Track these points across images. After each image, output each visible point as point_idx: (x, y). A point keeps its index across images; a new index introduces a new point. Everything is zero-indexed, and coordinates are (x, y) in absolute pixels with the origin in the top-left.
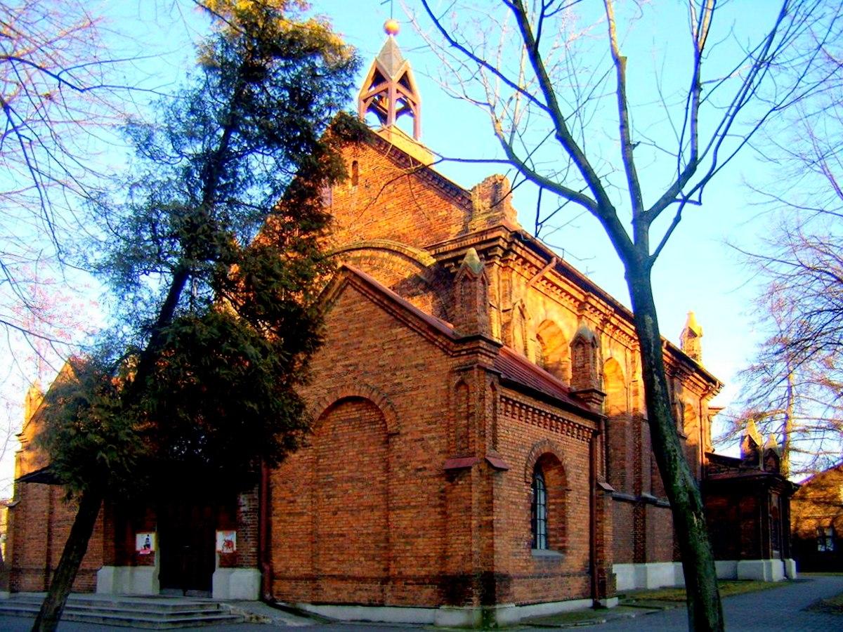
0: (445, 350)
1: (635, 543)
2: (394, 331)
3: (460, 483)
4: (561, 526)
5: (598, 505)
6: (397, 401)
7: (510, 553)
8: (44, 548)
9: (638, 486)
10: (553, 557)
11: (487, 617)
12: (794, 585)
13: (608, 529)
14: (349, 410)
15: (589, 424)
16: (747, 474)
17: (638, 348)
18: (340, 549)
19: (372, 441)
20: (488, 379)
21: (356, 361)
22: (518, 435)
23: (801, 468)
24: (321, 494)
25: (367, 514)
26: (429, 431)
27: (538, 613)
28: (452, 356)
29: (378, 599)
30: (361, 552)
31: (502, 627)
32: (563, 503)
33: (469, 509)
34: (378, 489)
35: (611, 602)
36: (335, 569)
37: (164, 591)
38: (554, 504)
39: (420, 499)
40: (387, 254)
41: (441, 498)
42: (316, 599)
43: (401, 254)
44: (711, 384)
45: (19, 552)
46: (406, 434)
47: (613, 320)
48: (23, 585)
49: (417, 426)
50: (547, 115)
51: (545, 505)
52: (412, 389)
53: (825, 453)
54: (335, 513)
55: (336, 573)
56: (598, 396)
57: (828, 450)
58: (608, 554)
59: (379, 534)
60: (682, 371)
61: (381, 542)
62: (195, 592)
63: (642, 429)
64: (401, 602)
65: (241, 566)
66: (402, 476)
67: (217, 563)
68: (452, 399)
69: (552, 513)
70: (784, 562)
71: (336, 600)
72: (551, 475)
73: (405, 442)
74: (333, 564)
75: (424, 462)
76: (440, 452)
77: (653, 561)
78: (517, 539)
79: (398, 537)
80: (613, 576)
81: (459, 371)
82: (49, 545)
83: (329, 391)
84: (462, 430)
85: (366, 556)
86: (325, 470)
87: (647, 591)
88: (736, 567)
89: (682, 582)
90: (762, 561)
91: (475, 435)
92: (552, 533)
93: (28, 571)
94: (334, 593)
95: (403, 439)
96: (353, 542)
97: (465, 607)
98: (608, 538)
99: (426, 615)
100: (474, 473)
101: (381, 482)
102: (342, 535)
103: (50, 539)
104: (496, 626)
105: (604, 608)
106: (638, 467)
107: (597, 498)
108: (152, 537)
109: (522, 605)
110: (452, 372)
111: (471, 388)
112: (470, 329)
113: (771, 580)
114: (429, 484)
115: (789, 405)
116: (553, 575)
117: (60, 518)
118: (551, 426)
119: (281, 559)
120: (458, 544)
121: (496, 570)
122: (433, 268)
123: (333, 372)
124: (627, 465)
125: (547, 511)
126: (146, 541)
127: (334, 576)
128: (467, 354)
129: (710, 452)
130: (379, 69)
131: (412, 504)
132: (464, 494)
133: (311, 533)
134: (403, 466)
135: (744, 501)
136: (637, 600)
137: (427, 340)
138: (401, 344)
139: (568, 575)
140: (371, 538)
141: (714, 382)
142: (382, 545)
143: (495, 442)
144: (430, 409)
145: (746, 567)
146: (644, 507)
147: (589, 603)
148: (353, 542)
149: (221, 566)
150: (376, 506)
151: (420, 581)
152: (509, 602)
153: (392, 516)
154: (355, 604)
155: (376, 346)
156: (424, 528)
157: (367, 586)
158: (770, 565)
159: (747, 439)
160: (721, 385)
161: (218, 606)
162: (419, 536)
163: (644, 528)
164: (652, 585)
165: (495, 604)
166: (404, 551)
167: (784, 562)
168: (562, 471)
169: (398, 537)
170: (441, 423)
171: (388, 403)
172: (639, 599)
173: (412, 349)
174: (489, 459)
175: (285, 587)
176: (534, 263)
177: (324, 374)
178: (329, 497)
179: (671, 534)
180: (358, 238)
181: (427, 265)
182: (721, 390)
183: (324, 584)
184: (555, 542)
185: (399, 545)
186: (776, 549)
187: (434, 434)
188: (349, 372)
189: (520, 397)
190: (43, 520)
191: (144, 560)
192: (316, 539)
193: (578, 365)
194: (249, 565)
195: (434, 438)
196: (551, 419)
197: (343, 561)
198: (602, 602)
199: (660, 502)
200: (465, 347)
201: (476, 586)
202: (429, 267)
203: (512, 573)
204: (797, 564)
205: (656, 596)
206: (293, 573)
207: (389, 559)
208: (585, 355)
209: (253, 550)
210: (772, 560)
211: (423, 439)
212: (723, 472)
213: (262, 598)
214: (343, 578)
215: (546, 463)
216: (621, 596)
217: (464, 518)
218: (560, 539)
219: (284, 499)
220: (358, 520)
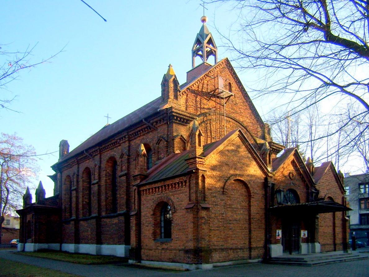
74: (325, 241)
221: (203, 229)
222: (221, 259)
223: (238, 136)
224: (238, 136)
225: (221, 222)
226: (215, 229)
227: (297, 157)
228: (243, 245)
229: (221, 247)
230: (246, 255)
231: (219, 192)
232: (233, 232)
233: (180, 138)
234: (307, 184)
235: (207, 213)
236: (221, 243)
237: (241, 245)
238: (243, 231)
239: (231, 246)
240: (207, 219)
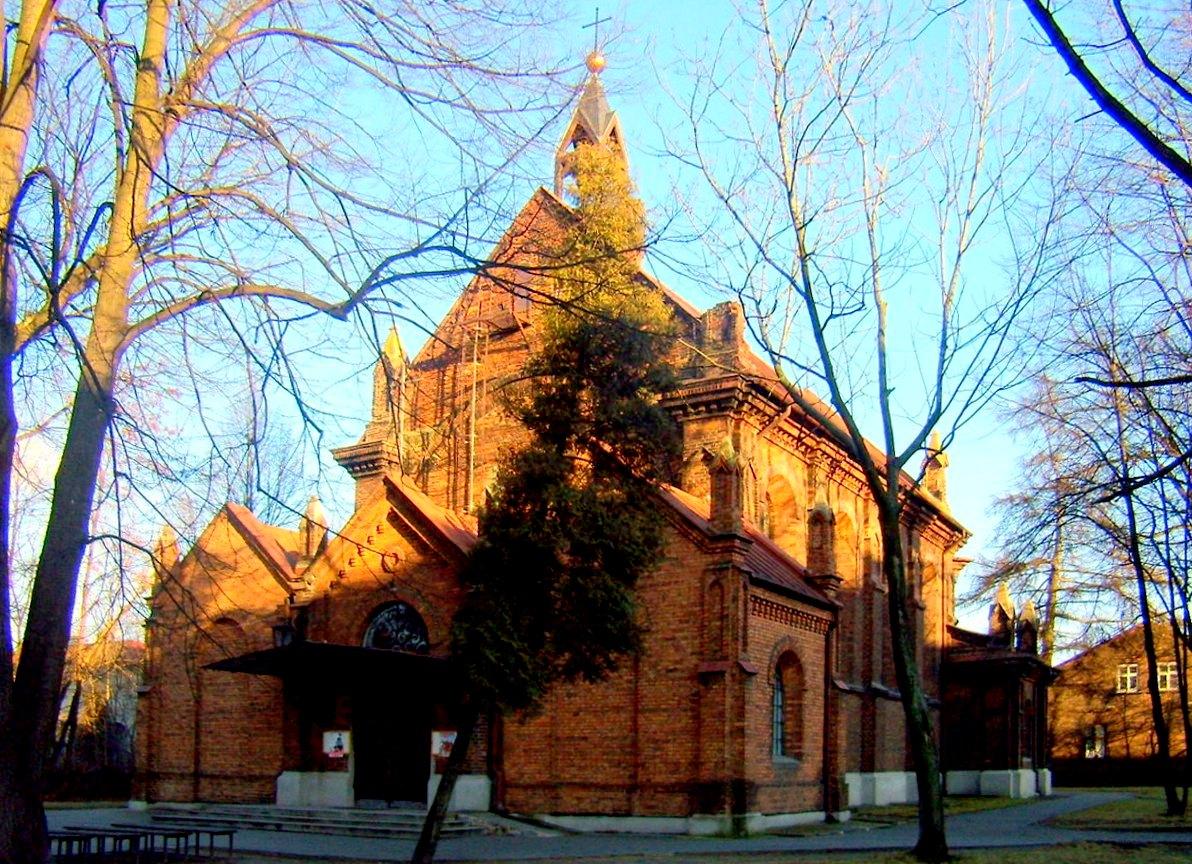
0: (700, 546)
1: (863, 747)
4: (797, 730)
5: (833, 706)
7: (760, 762)
8: (189, 745)
9: (867, 678)
10: (790, 764)
11: (739, 829)
12: (1049, 802)
13: (842, 733)
15: (825, 615)
16: (995, 656)
17: (871, 496)
18: (583, 755)
20: (742, 579)
22: (765, 633)
23: (1069, 641)
25: (612, 715)
26: (681, 630)
27: (777, 825)
28: (706, 553)
29: (624, 808)
31: (753, 836)
32: (800, 705)
33: (722, 714)
34: (624, 689)
35: (844, 816)
36: (575, 776)
37: (362, 802)
38: (791, 705)
41: (692, 701)
44: (955, 532)
45: (154, 750)
46: (657, 632)
47: (844, 465)
48: (162, 794)
49: (669, 624)
50: (801, 298)
51: (781, 707)
52: (664, 584)
53: (1099, 621)
55: (577, 780)
56: (833, 581)
57: (1103, 617)
58: (842, 761)
59: (625, 738)
60: (922, 520)
62: (403, 803)
63: (874, 601)
64: (651, 811)
65: (469, 773)
66: (652, 676)
67: (433, 769)
68: (707, 598)
69: (789, 716)
70: (1037, 773)
71: (577, 810)
72: (789, 673)
73: (656, 640)
74: (573, 770)
75: (676, 662)
76: (692, 654)
77: (883, 770)
78: (760, 745)
79: (648, 741)
80: (846, 787)
81: (714, 570)
82: (198, 743)
84: (715, 633)
87: (873, 806)
88: (979, 777)
89: (916, 798)
90: (1010, 772)
91: (728, 638)
92: (789, 737)
93: (168, 776)
98: (843, 743)
99: (676, 824)
100: (728, 677)
102: (585, 739)
103: (197, 736)
104: (747, 836)
105: (838, 822)
106: (868, 648)
107: (833, 699)
108: (346, 738)
109: (767, 815)
110: (705, 571)
111: (726, 589)
112: (725, 526)
113: (1018, 797)
115: (1056, 552)
116: (790, 784)
117: (211, 709)
118: (792, 621)
119: (514, 765)
120: (711, 751)
121: (746, 777)
124: (856, 646)
125: (784, 713)
126: (336, 742)
127: (575, 784)
128: (722, 552)
129: (952, 624)
131: (663, 707)
132: (718, 699)
133: (550, 736)
134: (654, 666)
135: (992, 692)
136: (869, 815)
137: (680, 533)
139: (803, 784)
141: (961, 532)
142: (628, 750)
143: (745, 644)
144: (682, 607)
145: (990, 779)
146: (874, 702)
147: (821, 816)
151: (670, 789)
152: (756, 811)
153: (641, 720)
154: (598, 814)
157: (611, 794)
158: (1018, 777)
159: (997, 609)
160: (968, 535)
161: (456, 817)
162: (668, 741)
163: (873, 727)
164: (881, 800)
165: (745, 812)
166: (654, 757)
167: (1037, 773)
168: (800, 670)
169: (648, 741)
172: (867, 814)
174: (741, 662)
175: (520, 796)
176: (762, 408)
178: (569, 695)
179: (903, 734)
182: (969, 540)
183: (563, 792)
184: (791, 748)
185: (647, 750)
186: (1028, 756)
187: (686, 634)
189: (767, 594)
190: (187, 711)
191: (337, 765)
192: (553, 743)
193: (816, 545)
194: (479, 772)
195: (686, 638)
196: (792, 614)
198: (835, 815)
199: (891, 693)
200: (720, 545)
201: (722, 794)
203: (758, 782)
204: (1053, 777)
205: (887, 812)
206: (528, 781)
207: (636, 765)
208: (823, 535)
209: (484, 754)
210: (1020, 771)
211: (674, 639)
212: (968, 652)
213: (493, 809)
214: (585, 786)
215: (788, 660)
216: (854, 810)
218: (796, 744)
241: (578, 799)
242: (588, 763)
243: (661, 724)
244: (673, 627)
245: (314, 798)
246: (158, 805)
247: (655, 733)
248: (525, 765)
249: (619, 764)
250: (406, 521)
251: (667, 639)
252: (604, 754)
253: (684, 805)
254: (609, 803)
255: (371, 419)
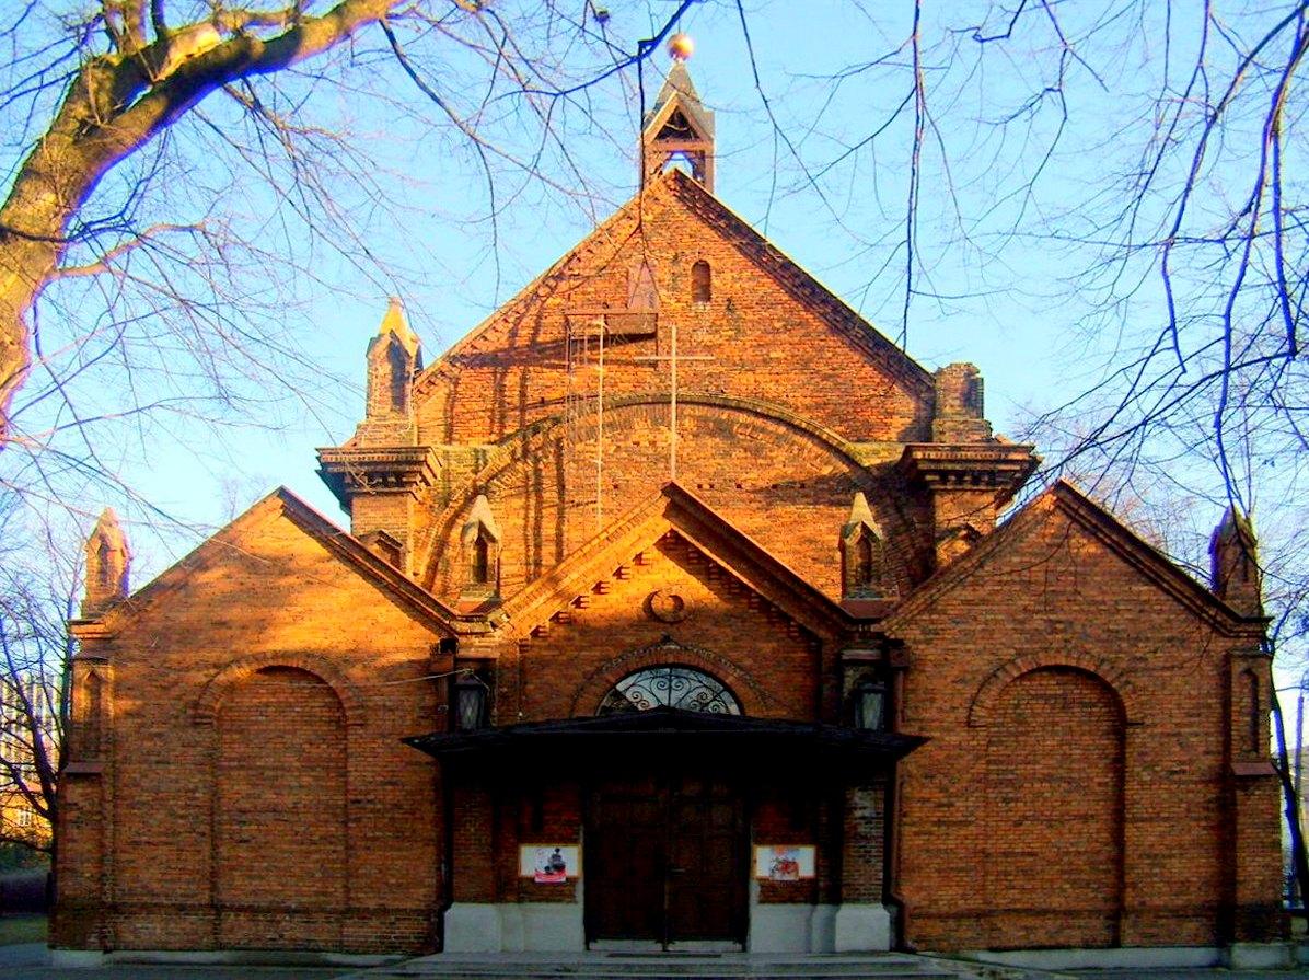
2: (1135, 588)
3: (1257, 792)
6: (1141, 680)
14: (1044, 682)
19: (1087, 728)
21: (1071, 617)
24: (993, 795)
25: (1077, 825)
26: (1190, 725)
30: (1066, 876)
36: (1014, 901)
37: (593, 946)
39: (1176, 810)
40: (782, 429)
42: (996, 943)
43: (811, 435)
46: (1155, 725)
52: (1164, 668)
54: (1018, 824)
61: (1101, 863)
64: (1155, 941)
65: (855, 901)
71: (1023, 942)
73: (1152, 736)
74: (1013, 894)
75: (1182, 763)
83: (1020, 653)
85: (1074, 882)
86: (1002, 762)
94: (1022, 933)
95: (1149, 731)
96: (1050, 863)
97: (1272, 944)
101: (1100, 784)
114: (1189, 791)
119: (920, 889)
122: (875, 473)
123: (1027, 627)
127: (1016, 910)
128: (1248, 637)
130: (683, 109)
131: (1163, 815)
134: (1150, 766)
138: (1147, 607)
140: (1084, 858)
144: (1190, 697)
148: (1050, 863)
149: (761, 902)
150: (1092, 816)
151: (1180, 914)
154: (1069, 947)
155: (1104, 603)
156: (1181, 846)
157: (1076, 922)
170: (1207, 717)
171: (1128, 683)
173: (1164, 616)
177: (1010, 626)
180: (712, 389)
181: (866, 465)
188: (1054, 631)
194: (869, 899)
197: (1033, 890)
202: (867, 470)
217: (1262, 835)
219: (929, 800)
220: (1061, 834)
221: (74, 841)
222: (172, 939)
223: (284, 514)
224: (284, 514)
225: (182, 817)
226: (154, 839)
227: (696, 521)
228: (313, 899)
229: (181, 900)
230: (325, 937)
231: (177, 718)
232: (253, 849)
233: (378, 542)
234: (801, 628)
235: (89, 790)
236: (181, 888)
237: (304, 900)
238: (313, 847)
239: (247, 901)
240: (88, 808)
241: (1026, 928)
242: (1037, 884)
243: (1162, 835)
244: (1174, 721)
245: (518, 942)
246: (118, 955)
247: (1152, 846)
248: (939, 888)
249: (1088, 884)
250: (723, 563)
251: (1168, 735)
252: (1063, 872)
253: (1201, 932)
254: (1077, 933)
255: (363, 420)
